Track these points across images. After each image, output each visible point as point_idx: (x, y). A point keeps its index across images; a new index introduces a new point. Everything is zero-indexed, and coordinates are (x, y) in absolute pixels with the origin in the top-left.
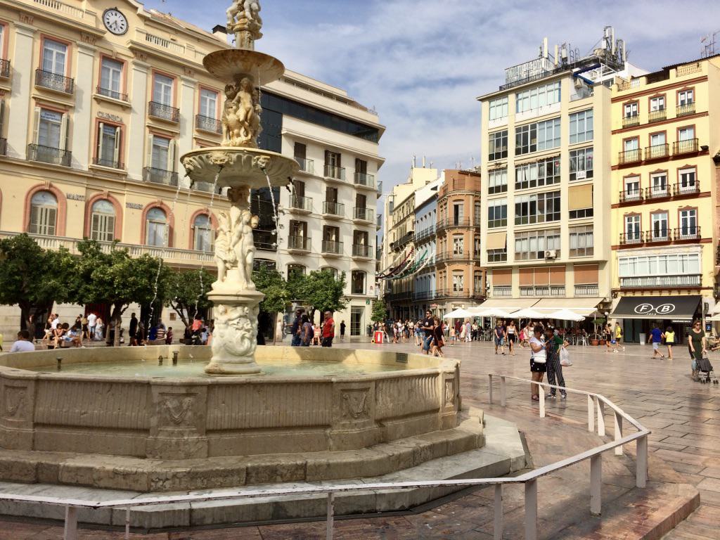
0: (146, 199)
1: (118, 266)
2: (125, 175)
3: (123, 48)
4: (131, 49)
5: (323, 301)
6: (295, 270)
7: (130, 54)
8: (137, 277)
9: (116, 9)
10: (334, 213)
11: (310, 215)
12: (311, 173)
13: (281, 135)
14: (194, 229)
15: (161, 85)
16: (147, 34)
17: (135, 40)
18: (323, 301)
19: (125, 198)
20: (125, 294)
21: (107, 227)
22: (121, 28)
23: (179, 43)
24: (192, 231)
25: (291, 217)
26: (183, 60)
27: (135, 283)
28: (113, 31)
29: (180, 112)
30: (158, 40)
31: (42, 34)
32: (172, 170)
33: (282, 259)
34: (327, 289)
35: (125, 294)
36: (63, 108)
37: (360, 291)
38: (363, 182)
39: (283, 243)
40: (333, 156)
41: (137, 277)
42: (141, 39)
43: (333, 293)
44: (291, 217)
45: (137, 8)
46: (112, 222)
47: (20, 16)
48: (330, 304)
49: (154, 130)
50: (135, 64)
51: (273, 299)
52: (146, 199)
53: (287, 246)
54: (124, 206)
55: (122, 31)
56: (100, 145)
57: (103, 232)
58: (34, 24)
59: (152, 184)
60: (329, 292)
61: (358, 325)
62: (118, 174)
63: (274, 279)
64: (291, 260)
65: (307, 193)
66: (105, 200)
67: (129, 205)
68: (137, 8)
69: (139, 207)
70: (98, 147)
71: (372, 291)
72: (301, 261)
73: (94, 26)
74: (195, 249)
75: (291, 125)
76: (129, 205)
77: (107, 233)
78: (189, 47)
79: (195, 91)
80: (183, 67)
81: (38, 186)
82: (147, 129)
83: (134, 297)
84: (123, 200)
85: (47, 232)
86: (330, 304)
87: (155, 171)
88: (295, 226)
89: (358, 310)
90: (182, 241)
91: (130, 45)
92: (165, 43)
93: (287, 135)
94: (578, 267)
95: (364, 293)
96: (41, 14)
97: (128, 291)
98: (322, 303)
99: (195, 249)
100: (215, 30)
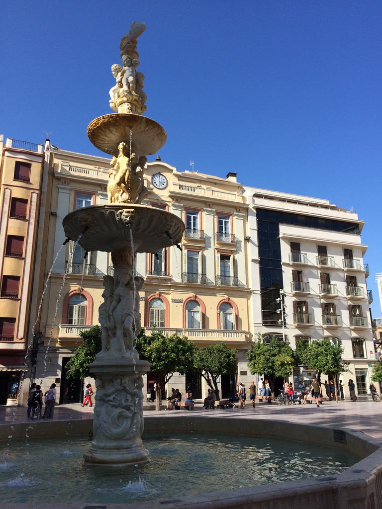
0: (185, 296)
1: (154, 345)
2: (170, 280)
3: (165, 196)
4: (170, 196)
5: (325, 365)
6: (302, 341)
7: (170, 200)
8: (168, 352)
9: (159, 174)
10: (329, 292)
11: (308, 296)
12: (333, 267)
13: (279, 239)
14: (220, 314)
15: (191, 216)
16: (180, 185)
17: (172, 190)
18: (325, 365)
19: (171, 296)
20: (160, 366)
21: (160, 316)
22: (163, 184)
23: (202, 188)
24: (219, 315)
25: (294, 299)
26: (201, 197)
27: (167, 357)
28: (158, 187)
29: (205, 232)
30: (188, 188)
31: (75, 191)
32: (201, 273)
33: (290, 332)
34: (327, 355)
35: (160, 366)
36: (199, 248)
37: (362, 356)
38: (351, 265)
39: (290, 318)
40: (322, 250)
41: (168, 352)
42: (176, 189)
43: (332, 358)
44: (294, 299)
45: (172, 170)
46: (163, 314)
47: (101, 187)
48: (331, 368)
49: (220, 251)
50: (173, 205)
51: (280, 365)
52: (185, 296)
53: (293, 322)
54: (170, 301)
55: (163, 186)
56: (153, 262)
57: (157, 321)
58: (70, 185)
59: (188, 284)
60: (329, 358)
61: (364, 385)
62: (165, 280)
63: (282, 349)
64: (298, 332)
65: (332, 282)
66: (157, 298)
67: (174, 301)
68: (172, 170)
69: (180, 301)
70: (152, 263)
71: (372, 355)
72: (307, 332)
73: (242, 202)
74: (222, 329)
75: (286, 230)
76: (174, 301)
77: (160, 321)
78: (208, 189)
79: (214, 217)
80: (205, 203)
81: (189, 298)
82: (216, 251)
83: (170, 367)
84: (170, 297)
85: (79, 323)
86: (331, 368)
87: (223, 277)
88: (298, 305)
89: (362, 372)
90: (213, 324)
91: (169, 194)
92: (193, 189)
93: (284, 238)
94: (155, 465)
95: (365, 357)
96: (214, 201)
97: (162, 363)
98: (324, 367)
99: (222, 329)
100: (228, 176)
